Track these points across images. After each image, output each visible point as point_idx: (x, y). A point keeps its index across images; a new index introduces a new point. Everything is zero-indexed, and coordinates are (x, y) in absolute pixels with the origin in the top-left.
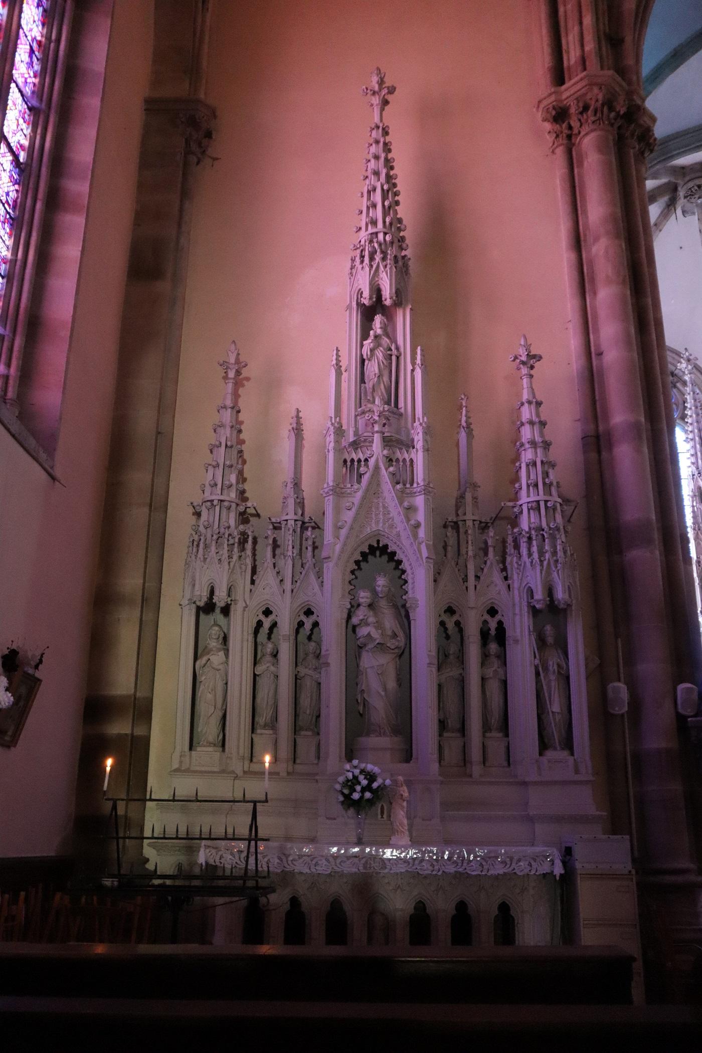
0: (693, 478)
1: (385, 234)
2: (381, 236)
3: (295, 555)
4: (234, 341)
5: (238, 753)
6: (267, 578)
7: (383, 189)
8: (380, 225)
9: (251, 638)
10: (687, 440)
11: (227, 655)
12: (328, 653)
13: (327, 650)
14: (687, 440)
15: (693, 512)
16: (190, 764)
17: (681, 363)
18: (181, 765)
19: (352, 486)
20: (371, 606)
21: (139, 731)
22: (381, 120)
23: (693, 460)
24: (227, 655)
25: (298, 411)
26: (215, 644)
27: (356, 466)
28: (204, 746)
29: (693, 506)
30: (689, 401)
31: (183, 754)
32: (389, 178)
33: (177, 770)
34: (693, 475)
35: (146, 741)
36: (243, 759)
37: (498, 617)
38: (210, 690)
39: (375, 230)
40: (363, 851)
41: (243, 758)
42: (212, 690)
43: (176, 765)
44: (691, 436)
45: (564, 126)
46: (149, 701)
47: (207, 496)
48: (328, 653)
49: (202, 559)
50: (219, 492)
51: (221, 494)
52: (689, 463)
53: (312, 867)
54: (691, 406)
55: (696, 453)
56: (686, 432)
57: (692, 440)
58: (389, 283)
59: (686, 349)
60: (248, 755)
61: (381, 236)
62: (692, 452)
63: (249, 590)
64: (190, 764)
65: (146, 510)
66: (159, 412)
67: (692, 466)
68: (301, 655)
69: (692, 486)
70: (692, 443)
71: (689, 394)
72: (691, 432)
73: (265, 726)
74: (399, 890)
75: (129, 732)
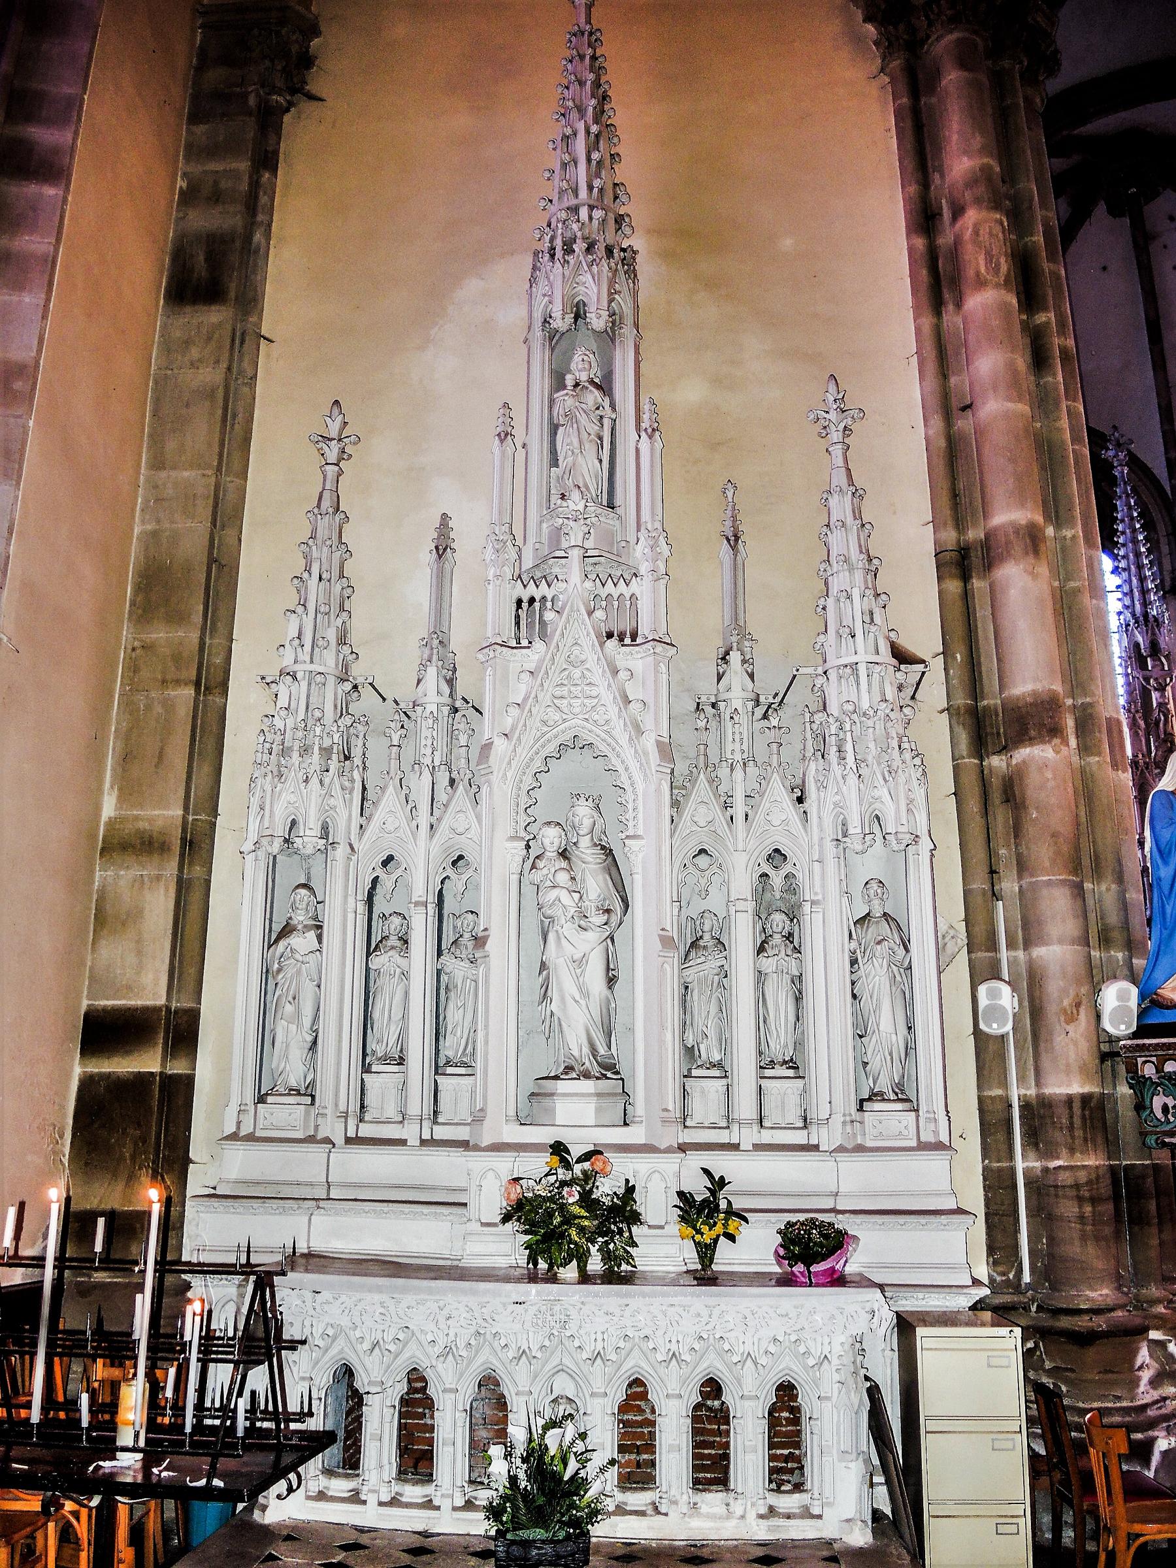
0: (1127, 630)
1: (591, 208)
2: (584, 213)
3: (437, 763)
4: (336, 402)
5: (336, 1105)
6: (389, 806)
7: (588, 132)
8: (583, 193)
9: (362, 908)
10: (1115, 571)
11: (320, 938)
12: (486, 933)
13: (486, 930)
14: (1115, 571)
15: (1128, 684)
16: (255, 1128)
17: (1107, 449)
18: (238, 1128)
19: (530, 643)
20: (564, 854)
21: (177, 1068)
22: (588, 22)
23: (1127, 602)
24: (320, 938)
25: (445, 517)
26: (301, 918)
27: (537, 609)
28: (281, 1095)
29: (1127, 675)
30: (1120, 509)
31: (243, 1108)
32: (599, 113)
33: (234, 1137)
34: (1128, 625)
35: (188, 1082)
36: (346, 1118)
37: (787, 868)
38: (290, 998)
39: (574, 202)
40: (54, 1494)
41: (345, 1116)
42: (294, 998)
43: (230, 1129)
44: (1123, 564)
45: (901, 27)
46: (193, 1016)
47: (288, 660)
48: (486, 933)
49: (275, 773)
50: (308, 659)
51: (312, 662)
52: (1119, 606)
53: (442, 1320)
54: (1123, 517)
55: (1132, 591)
56: (1115, 557)
57: (1124, 570)
58: (596, 291)
59: (1115, 428)
60: (354, 1106)
61: (584, 213)
62: (1126, 589)
63: (358, 827)
64: (255, 1128)
65: (190, 691)
66: (214, 523)
67: (1126, 611)
68: (448, 937)
69: (1125, 643)
70: (1125, 575)
71: (1120, 497)
72: (1123, 557)
73: (385, 1059)
74: (599, 1360)
75: (156, 1069)
